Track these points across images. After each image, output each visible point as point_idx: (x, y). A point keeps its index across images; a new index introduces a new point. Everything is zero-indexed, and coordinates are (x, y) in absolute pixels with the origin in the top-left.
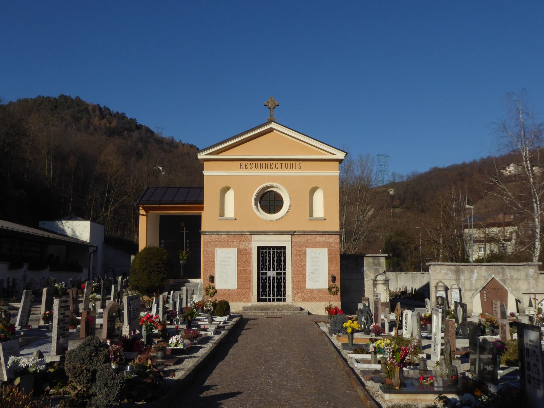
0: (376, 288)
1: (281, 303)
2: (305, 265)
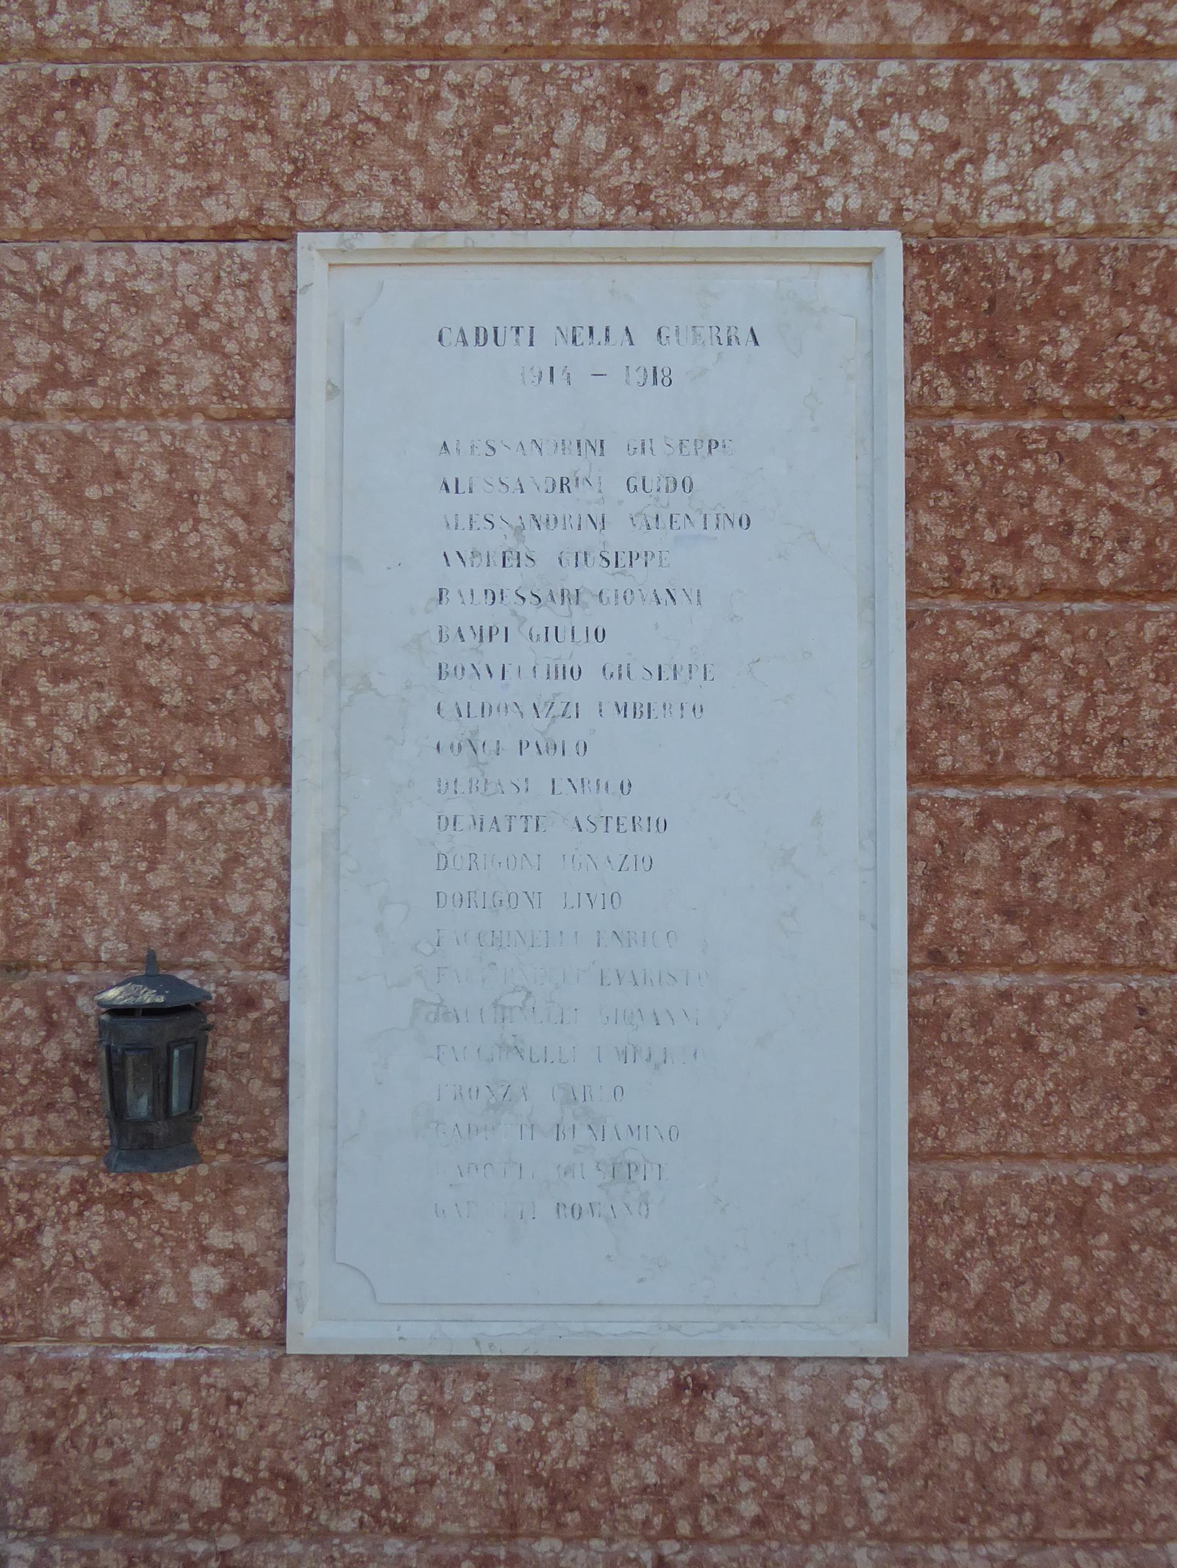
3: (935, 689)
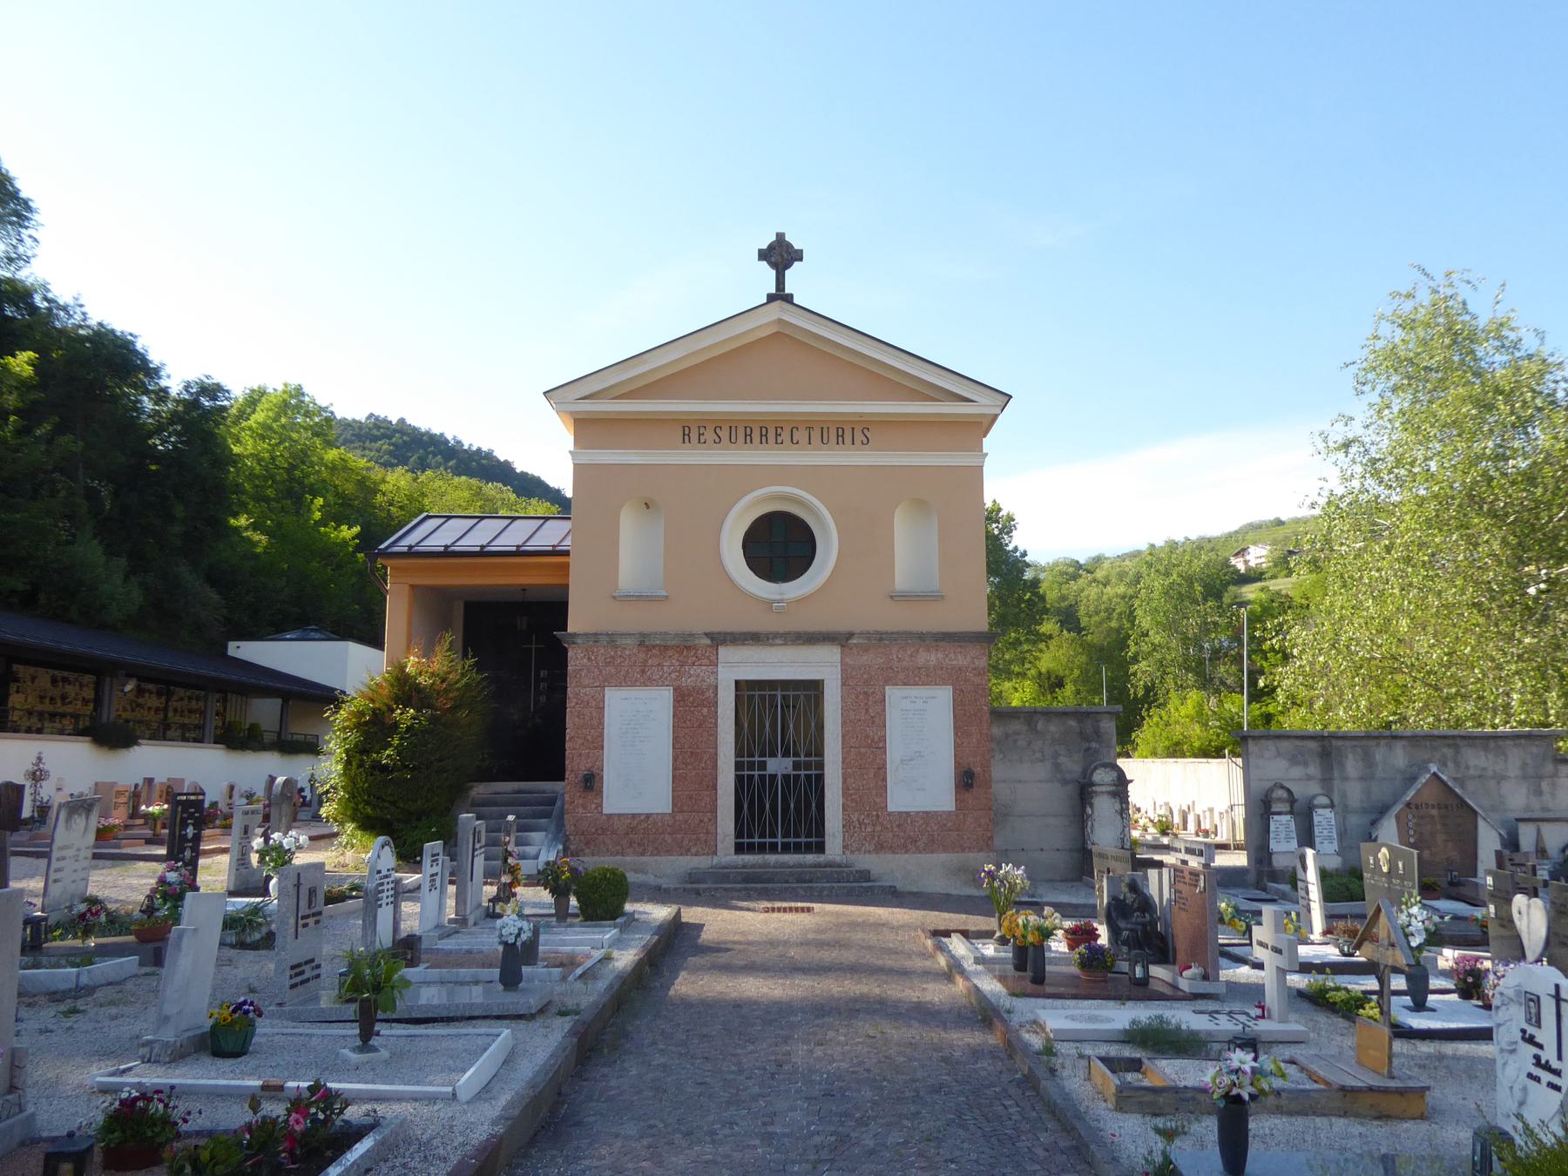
1: (810, 858)
3: (676, 739)
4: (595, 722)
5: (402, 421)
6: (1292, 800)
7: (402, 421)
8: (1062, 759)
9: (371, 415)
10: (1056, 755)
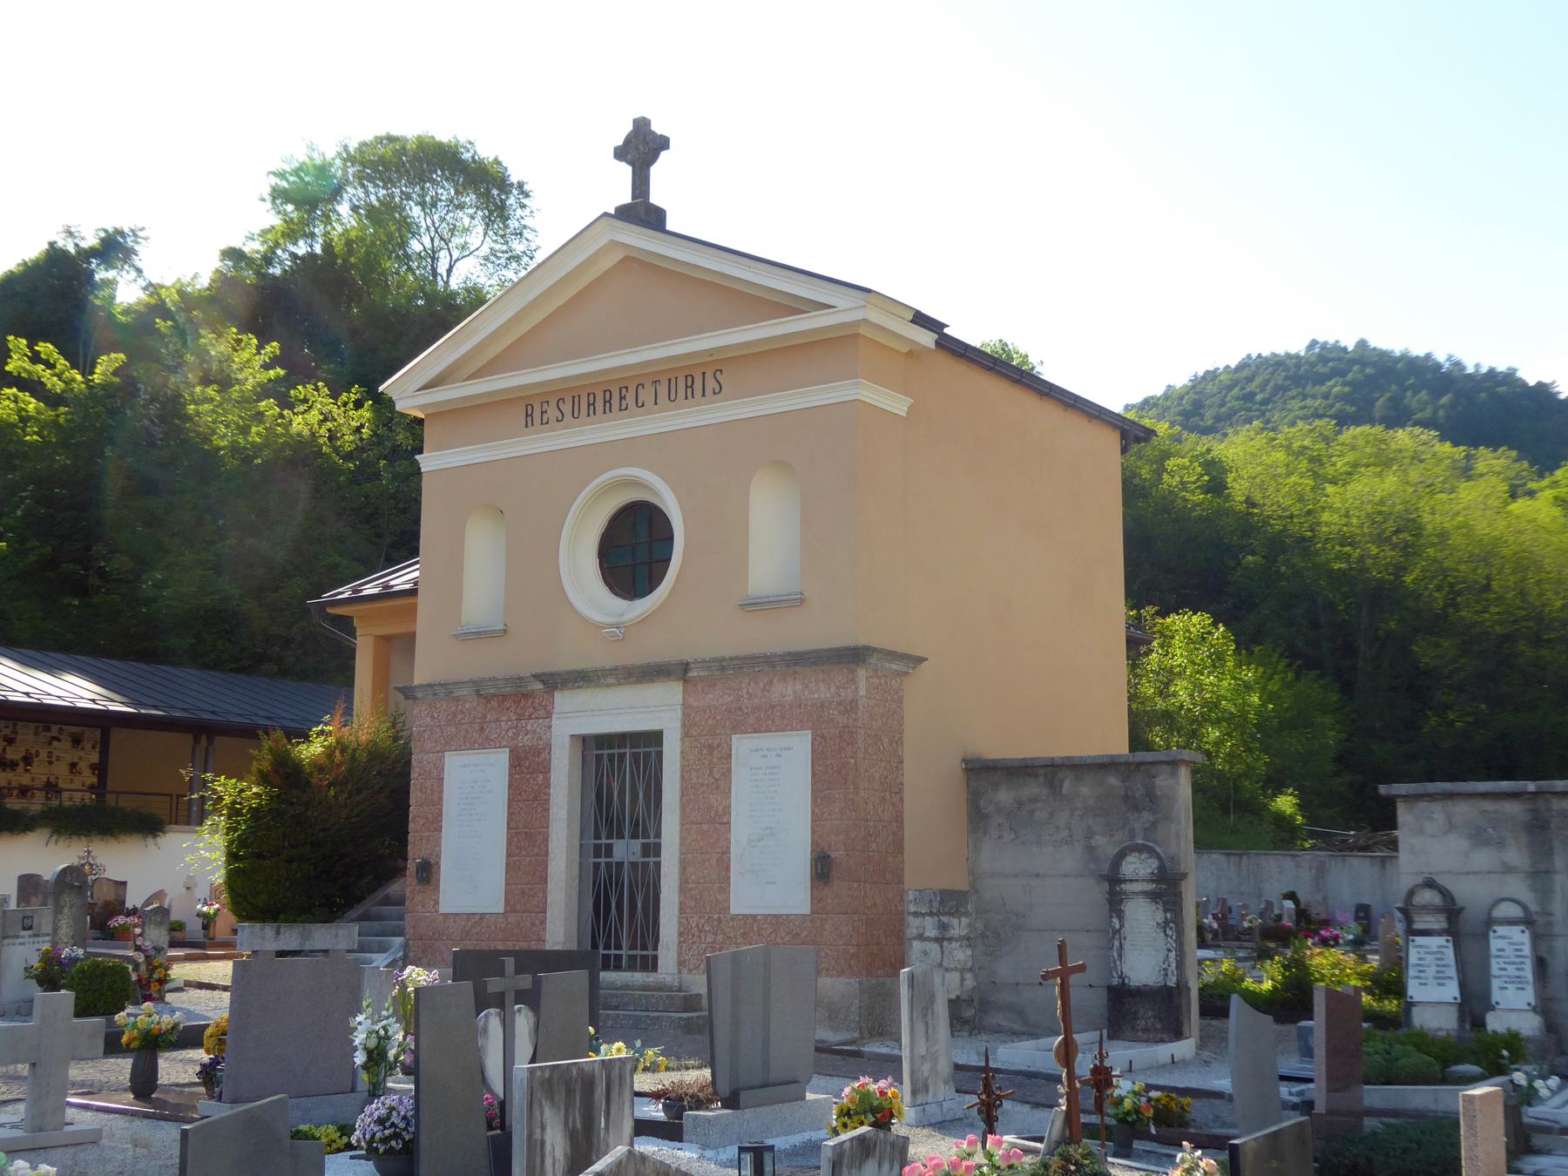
0: (1120, 916)
1: (638, 977)
2: (727, 811)
4: (435, 798)
5: (1362, 344)
6: (1452, 911)
7: (1362, 344)
8: (1099, 840)
9: (1314, 343)
10: (1089, 835)
